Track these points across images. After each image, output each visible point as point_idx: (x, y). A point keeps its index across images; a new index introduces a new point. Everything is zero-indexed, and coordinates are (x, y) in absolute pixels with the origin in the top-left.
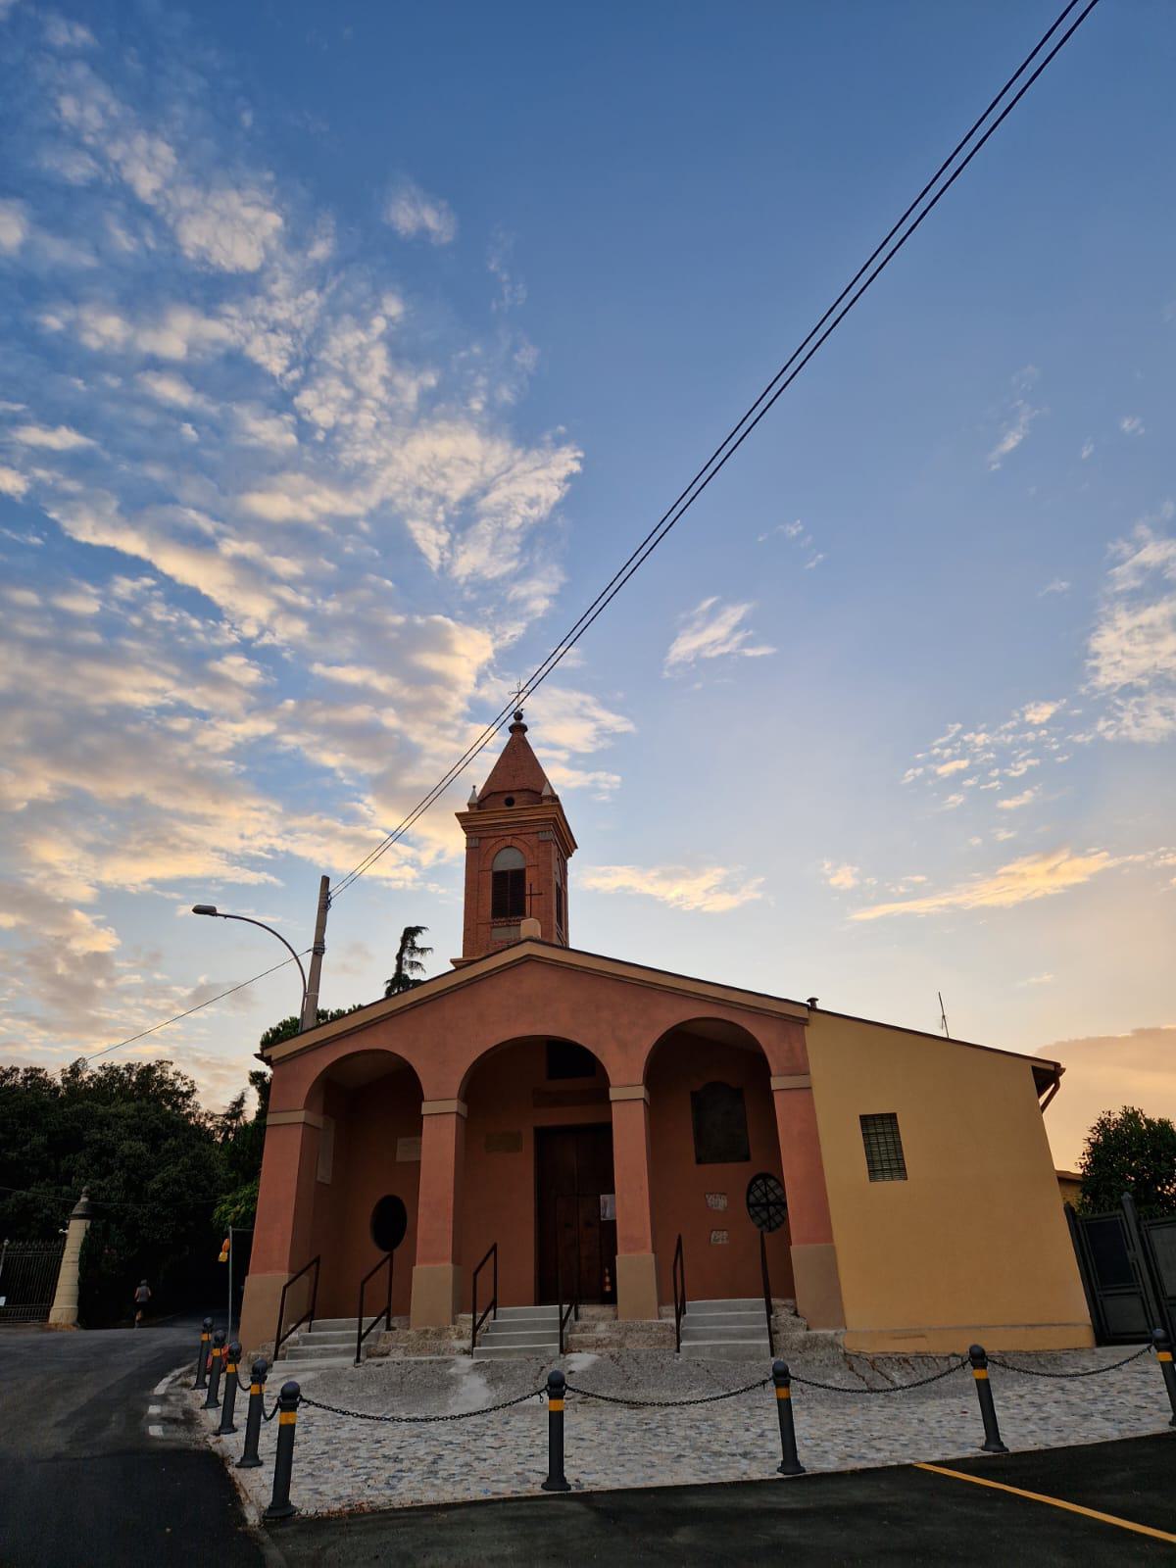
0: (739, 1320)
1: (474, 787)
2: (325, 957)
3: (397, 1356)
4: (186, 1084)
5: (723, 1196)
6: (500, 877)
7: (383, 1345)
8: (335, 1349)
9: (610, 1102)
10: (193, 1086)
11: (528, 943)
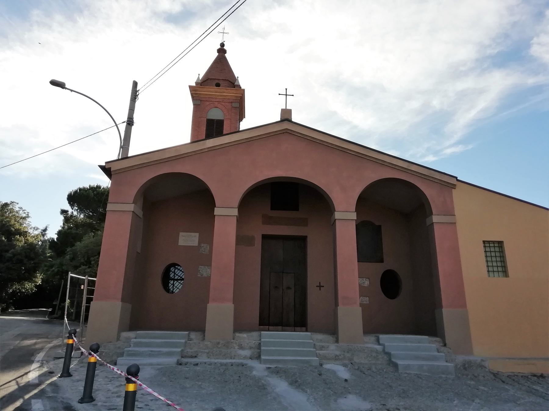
1: (199, 75)
4: (25, 213)
5: (367, 279)
6: (210, 122)
8: (160, 351)
9: (356, 211)
10: (28, 215)
11: (286, 121)
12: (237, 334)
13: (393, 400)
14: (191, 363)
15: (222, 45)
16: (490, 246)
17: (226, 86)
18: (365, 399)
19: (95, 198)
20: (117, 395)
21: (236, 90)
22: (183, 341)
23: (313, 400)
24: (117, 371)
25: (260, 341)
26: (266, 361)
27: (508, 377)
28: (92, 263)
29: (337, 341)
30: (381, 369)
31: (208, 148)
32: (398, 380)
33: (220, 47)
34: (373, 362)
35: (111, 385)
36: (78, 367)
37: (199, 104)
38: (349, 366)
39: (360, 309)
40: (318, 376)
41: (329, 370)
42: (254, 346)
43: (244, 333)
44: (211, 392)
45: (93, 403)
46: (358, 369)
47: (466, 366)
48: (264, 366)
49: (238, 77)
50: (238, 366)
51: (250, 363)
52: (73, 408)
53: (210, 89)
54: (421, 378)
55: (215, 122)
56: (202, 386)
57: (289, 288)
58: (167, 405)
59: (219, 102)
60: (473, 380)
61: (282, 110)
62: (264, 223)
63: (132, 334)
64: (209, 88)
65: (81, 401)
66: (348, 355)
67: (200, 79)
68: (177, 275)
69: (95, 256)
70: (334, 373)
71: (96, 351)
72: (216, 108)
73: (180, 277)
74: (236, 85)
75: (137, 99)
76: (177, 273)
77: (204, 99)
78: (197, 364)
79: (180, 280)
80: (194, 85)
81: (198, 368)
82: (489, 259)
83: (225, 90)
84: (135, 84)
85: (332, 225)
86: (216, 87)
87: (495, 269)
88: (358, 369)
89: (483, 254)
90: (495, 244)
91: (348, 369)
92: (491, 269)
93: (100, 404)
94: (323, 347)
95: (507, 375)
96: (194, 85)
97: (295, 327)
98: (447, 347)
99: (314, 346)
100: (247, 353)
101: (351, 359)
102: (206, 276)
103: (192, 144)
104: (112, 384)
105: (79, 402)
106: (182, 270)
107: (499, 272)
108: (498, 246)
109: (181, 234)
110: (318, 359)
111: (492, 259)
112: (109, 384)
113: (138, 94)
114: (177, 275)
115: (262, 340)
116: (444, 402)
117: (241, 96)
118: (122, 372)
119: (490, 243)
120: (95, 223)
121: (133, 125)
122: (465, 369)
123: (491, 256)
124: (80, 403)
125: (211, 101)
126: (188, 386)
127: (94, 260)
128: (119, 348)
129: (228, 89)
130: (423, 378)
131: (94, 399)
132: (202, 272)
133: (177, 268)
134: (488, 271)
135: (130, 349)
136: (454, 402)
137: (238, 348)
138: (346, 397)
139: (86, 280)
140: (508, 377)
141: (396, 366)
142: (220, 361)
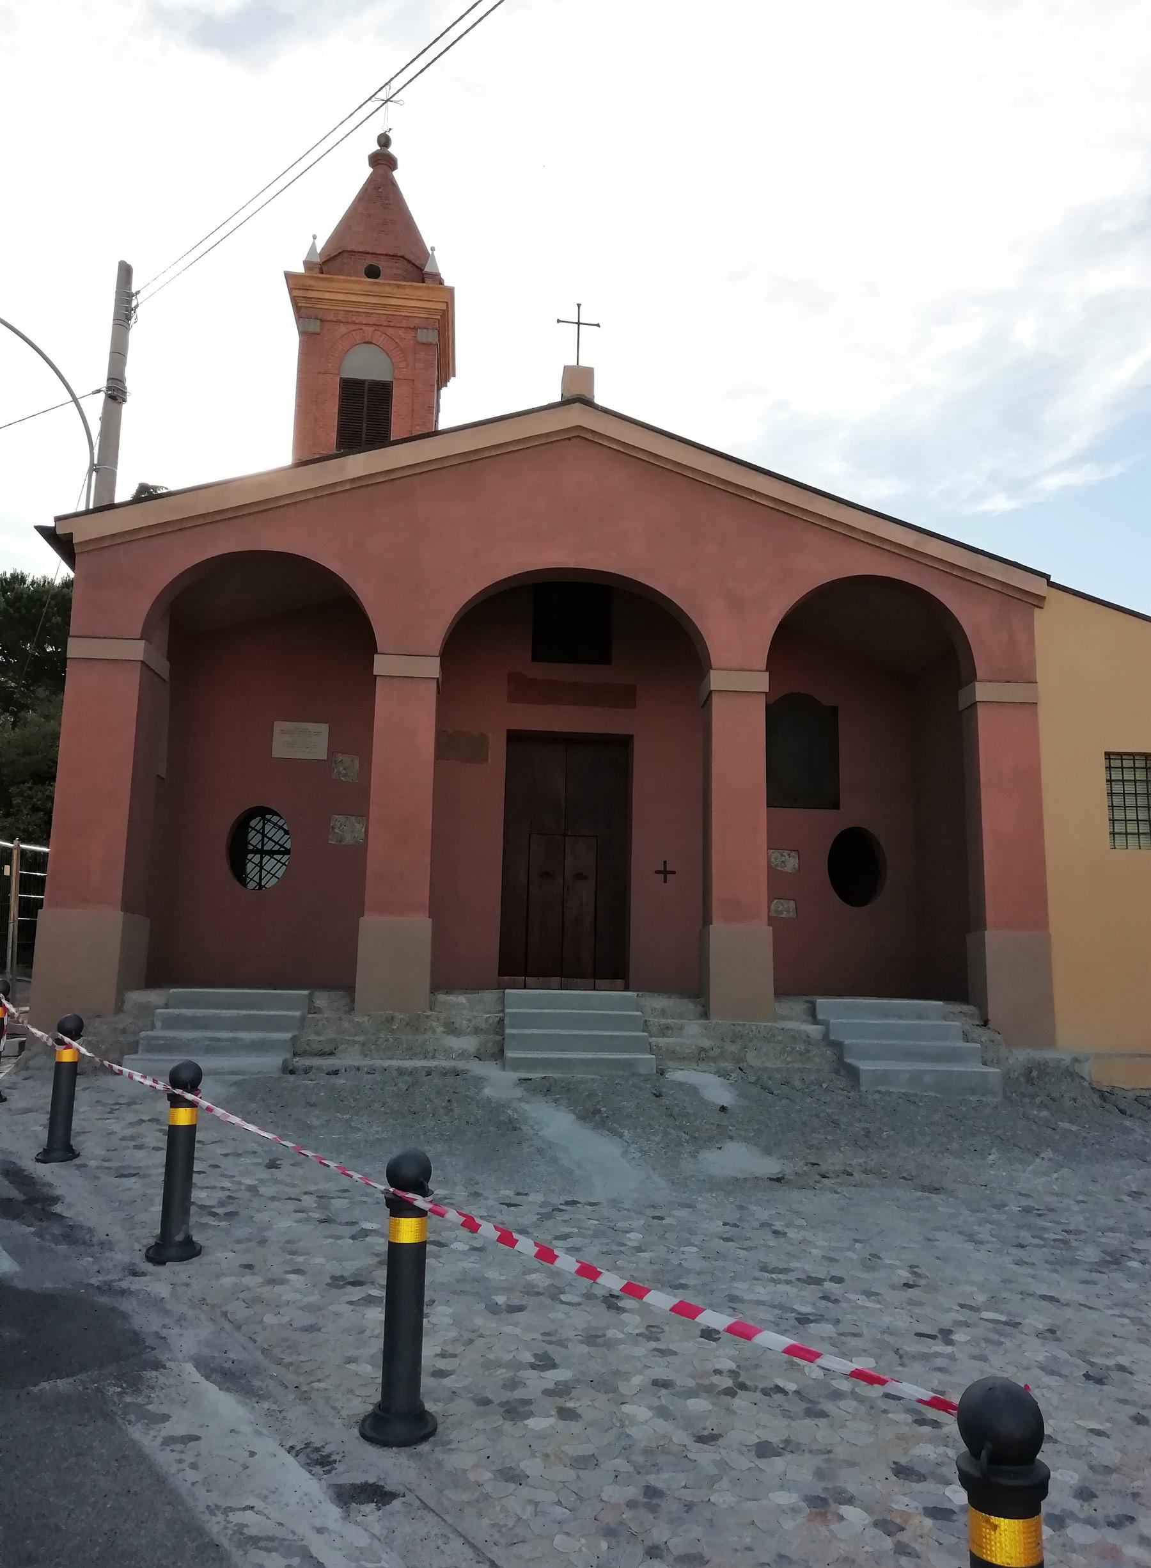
0: (605, 1022)
1: (315, 237)
2: (126, 408)
3: (350, 1058)
5: (793, 854)
6: (351, 389)
7: (313, 1037)
8: (234, 1040)
9: (767, 670)
12: (442, 997)
13: (837, 1153)
14: (319, 1069)
15: (384, 141)
16: (1122, 768)
17: (395, 277)
18: (768, 1151)
19: (11, 611)
20: (133, 1143)
21: (428, 288)
22: (297, 1014)
23: (638, 1155)
24: (142, 1080)
25: (501, 1015)
26: (518, 1064)
27: (1136, 1100)
28: (17, 801)
29: (705, 1015)
30: (815, 1081)
31: (353, 480)
32: (855, 1107)
33: (377, 148)
34: (796, 1065)
35: (115, 1121)
36: (14, 1078)
37: (318, 330)
38: (734, 1075)
39: (767, 932)
40: (654, 1097)
41: (681, 1085)
42: (483, 1026)
43: (461, 994)
44: (377, 1136)
45: (77, 1161)
46: (755, 1083)
47: (1035, 1074)
48: (514, 1075)
49: (433, 249)
50: (445, 1074)
51: (477, 1068)
52: (26, 1173)
53: (347, 286)
54: (914, 1103)
55: (366, 390)
56: (353, 1124)
57: (580, 876)
58: (266, 1166)
59: (376, 327)
60: (1048, 1108)
61: (567, 369)
62: (513, 698)
63: (154, 996)
64: (345, 281)
65: (45, 1157)
66: (732, 1048)
67: (319, 252)
68: (270, 839)
69: (23, 783)
70: (693, 1091)
71: (75, 1034)
72: (369, 345)
73: (279, 845)
74: (428, 274)
75: (133, 319)
76: (269, 835)
77: (331, 317)
78: (336, 1072)
79: (278, 852)
80: (300, 269)
81: (339, 1081)
82: (1117, 801)
83: (395, 290)
84: (125, 272)
85: (702, 707)
86: (369, 278)
87: (1131, 828)
88: (755, 1083)
89: (1104, 788)
90: (1136, 761)
91: (730, 1083)
92: (1119, 828)
93: (93, 1163)
94: (668, 1028)
95: (1134, 1097)
96: (300, 269)
97: (595, 978)
98: (989, 1028)
99: (646, 1026)
100: (469, 1043)
101: (738, 1059)
102: (352, 842)
103: (300, 468)
104: (116, 1118)
105: (38, 1160)
106: (285, 827)
107: (1141, 836)
108: (1144, 766)
109: (279, 726)
110: (653, 1056)
111: (1124, 801)
112: (109, 1119)
113: (134, 303)
114: (270, 839)
115: (508, 1010)
116: (964, 1158)
117: (444, 310)
118: (155, 1081)
119: (1124, 758)
120: (13, 685)
121: (125, 401)
122: (1030, 1080)
123: (1136, 794)
124: (42, 1163)
125: (354, 323)
126: (316, 1123)
127: (20, 794)
128: (124, 1031)
129: (403, 287)
130: (921, 1104)
131: (77, 1153)
132: (341, 833)
133: (269, 820)
134: (1113, 834)
135: (152, 1033)
136: (990, 1157)
137: (444, 1032)
138: (720, 1148)
139: (15, 852)
140: (1136, 1100)
141: (853, 1073)
142: (395, 1063)
